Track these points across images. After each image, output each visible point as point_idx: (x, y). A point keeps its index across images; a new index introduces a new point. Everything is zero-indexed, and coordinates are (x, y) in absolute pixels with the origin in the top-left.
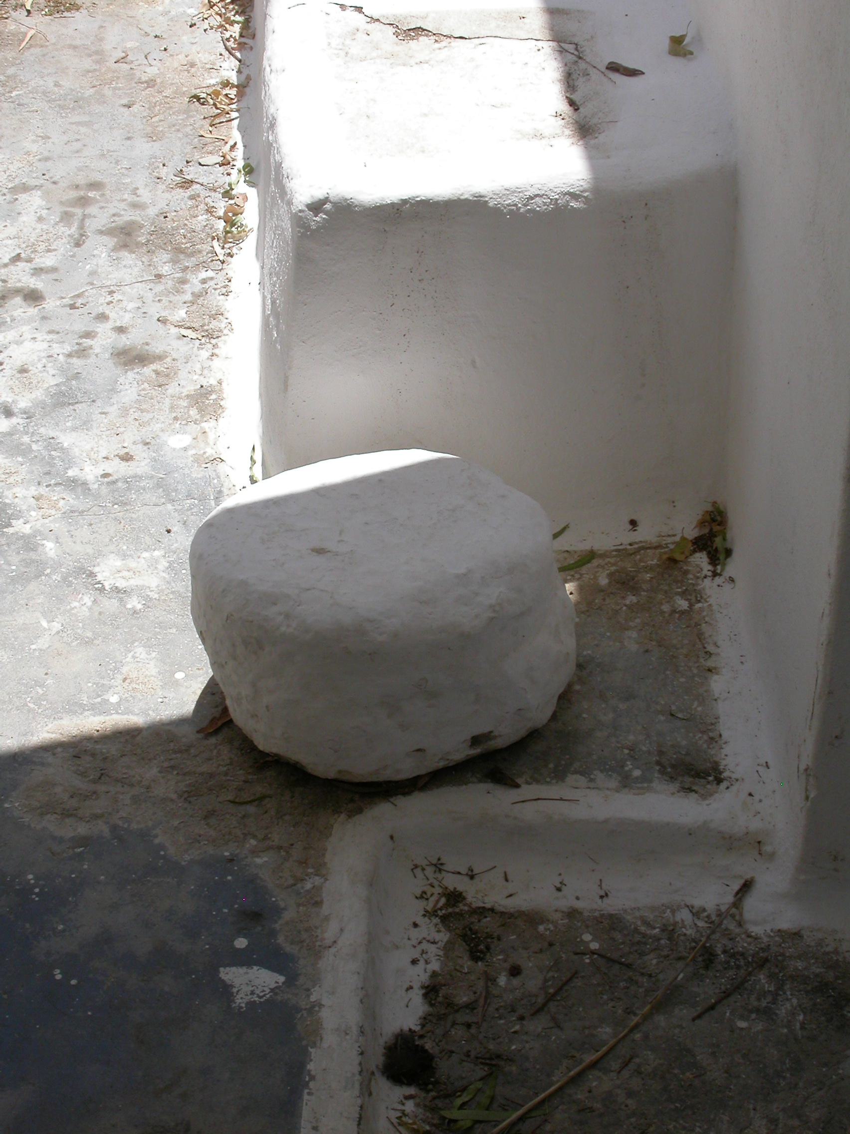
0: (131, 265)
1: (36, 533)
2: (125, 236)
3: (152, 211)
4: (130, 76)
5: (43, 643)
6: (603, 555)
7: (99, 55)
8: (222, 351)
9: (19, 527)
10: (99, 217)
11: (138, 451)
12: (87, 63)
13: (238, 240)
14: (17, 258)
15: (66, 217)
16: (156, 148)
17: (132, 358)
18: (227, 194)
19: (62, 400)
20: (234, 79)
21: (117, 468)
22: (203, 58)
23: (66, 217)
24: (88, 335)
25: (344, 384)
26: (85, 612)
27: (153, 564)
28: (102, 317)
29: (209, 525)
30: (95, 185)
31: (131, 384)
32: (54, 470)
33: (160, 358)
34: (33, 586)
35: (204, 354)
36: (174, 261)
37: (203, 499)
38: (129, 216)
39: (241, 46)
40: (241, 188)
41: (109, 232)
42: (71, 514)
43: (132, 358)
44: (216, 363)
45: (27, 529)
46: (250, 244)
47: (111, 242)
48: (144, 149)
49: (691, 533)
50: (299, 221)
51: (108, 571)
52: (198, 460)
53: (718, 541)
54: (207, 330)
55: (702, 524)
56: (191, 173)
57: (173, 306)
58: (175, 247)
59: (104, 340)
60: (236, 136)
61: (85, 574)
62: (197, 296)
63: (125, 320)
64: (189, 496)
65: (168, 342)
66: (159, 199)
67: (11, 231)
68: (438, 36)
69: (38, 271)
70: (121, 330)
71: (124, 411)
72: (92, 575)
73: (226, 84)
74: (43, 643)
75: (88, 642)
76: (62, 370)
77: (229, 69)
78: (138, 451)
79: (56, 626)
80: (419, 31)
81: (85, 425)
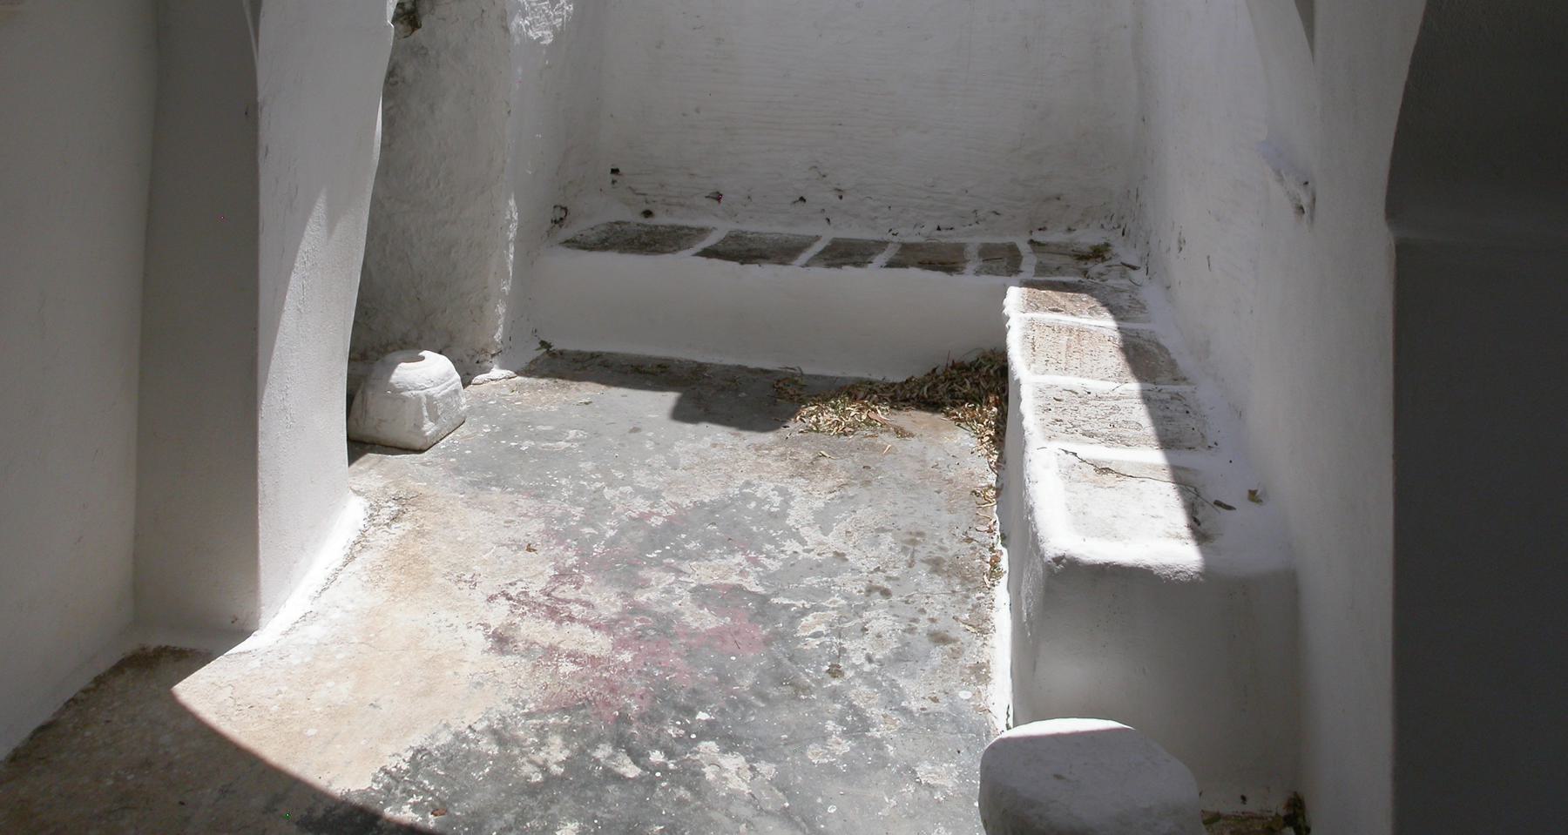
0: (938, 584)
1: (883, 738)
2: (936, 565)
3: (951, 553)
4: (939, 476)
5: (884, 812)
6: (1226, 818)
7: (923, 462)
8: (989, 642)
9: (874, 733)
10: (922, 553)
11: (941, 696)
12: (917, 466)
13: (999, 575)
14: (878, 569)
15: (904, 550)
16: (953, 517)
17: (940, 638)
18: (992, 549)
19: (900, 657)
20: (994, 483)
21: (927, 704)
22: (978, 471)
23: (904, 550)
24: (915, 620)
25: (1067, 670)
26: (910, 796)
27: (950, 771)
28: (923, 611)
29: (992, 747)
30: (920, 534)
31: (938, 654)
32: (893, 699)
33: (955, 641)
34: (880, 773)
35: (979, 643)
36: (962, 584)
37: (979, 735)
38: (938, 554)
39: (998, 467)
40: (999, 547)
41: (927, 562)
42: (903, 729)
43: (940, 638)
44: (986, 649)
45: (878, 735)
46: (1004, 580)
47: (929, 568)
48: (946, 517)
49: (1283, 812)
50: (1048, 567)
51: (924, 771)
52: (976, 708)
53: (1300, 820)
54: (982, 627)
55: (1288, 806)
56: (972, 534)
57: (962, 611)
58: (967, 578)
59: (923, 625)
60: (996, 517)
61: (909, 771)
62: (975, 607)
63: (936, 614)
64: (971, 731)
65: (958, 632)
66: (954, 547)
67: (875, 553)
68: (1119, 474)
69: (888, 579)
70: (933, 620)
71: (934, 671)
72: (914, 772)
73: (990, 487)
74: (884, 812)
75: (911, 817)
76: (901, 640)
77: (992, 479)
78: (941, 696)
79: (894, 802)
80: (1108, 470)
81: (911, 675)
